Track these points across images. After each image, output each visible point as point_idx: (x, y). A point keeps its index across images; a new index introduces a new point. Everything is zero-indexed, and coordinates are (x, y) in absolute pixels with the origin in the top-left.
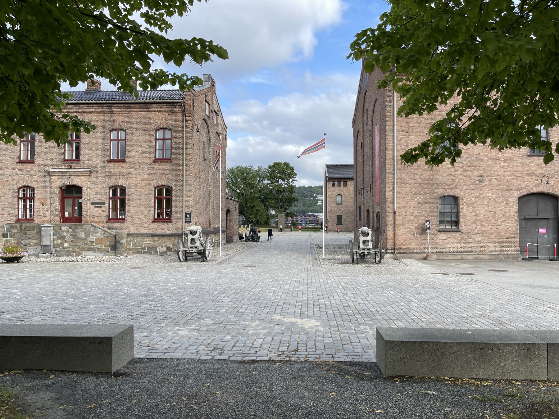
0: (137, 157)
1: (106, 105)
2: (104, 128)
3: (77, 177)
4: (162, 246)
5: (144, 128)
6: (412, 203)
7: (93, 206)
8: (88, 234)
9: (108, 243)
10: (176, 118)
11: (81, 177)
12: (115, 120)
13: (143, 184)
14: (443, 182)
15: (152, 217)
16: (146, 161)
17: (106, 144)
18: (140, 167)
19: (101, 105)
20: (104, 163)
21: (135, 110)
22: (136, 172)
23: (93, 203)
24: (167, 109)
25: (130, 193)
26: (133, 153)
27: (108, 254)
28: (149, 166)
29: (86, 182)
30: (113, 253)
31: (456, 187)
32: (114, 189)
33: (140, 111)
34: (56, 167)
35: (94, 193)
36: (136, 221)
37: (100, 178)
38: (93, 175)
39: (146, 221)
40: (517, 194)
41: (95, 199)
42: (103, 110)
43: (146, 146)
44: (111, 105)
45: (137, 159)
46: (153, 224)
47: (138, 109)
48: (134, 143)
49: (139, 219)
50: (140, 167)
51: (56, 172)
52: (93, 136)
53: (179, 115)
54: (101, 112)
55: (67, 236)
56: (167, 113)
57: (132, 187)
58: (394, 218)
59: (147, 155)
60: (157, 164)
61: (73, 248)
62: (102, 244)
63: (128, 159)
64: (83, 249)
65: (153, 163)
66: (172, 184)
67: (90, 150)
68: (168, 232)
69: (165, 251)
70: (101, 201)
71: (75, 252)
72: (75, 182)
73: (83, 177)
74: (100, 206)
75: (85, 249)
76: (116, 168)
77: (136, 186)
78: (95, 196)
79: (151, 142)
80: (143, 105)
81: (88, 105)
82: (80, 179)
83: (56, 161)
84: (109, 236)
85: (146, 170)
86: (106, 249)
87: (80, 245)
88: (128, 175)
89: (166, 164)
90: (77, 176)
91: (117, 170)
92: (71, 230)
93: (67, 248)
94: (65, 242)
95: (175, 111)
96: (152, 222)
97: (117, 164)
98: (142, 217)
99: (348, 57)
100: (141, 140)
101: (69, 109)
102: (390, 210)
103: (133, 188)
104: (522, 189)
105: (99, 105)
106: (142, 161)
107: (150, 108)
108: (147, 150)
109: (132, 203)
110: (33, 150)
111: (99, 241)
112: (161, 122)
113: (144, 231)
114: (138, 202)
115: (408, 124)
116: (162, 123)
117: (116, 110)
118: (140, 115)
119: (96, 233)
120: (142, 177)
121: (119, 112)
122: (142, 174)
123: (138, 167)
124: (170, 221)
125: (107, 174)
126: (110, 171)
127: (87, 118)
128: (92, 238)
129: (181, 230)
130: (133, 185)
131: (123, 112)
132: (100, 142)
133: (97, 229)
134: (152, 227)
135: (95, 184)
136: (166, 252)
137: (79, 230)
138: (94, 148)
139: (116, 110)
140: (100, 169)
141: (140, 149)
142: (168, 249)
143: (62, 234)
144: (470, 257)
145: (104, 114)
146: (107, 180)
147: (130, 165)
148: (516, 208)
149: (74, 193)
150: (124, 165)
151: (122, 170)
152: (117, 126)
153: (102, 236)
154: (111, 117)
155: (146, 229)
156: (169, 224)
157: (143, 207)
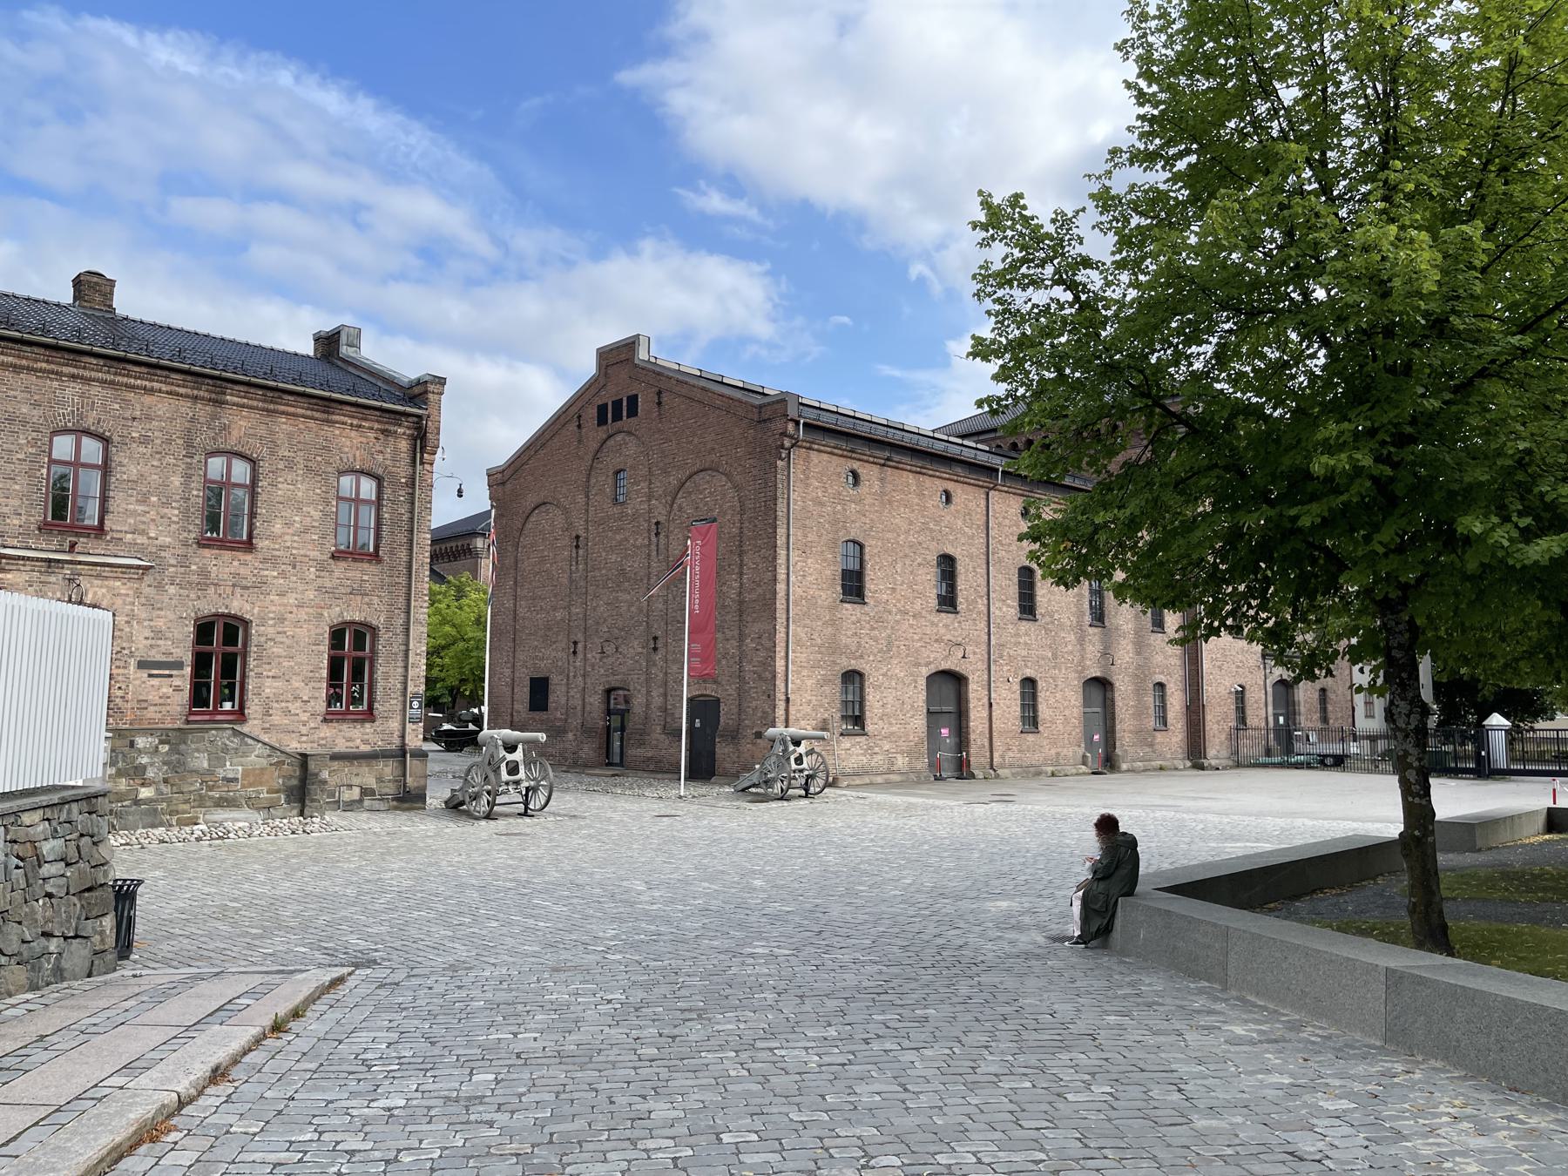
0: (287, 538)
1: (210, 382)
2: (189, 444)
3: (97, 582)
4: (350, 786)
5: (310, 464)
6: (809, 682)
7: (144, 674)
8: (218, 758)
9: (281, 781)
10: (396, 450)
11: (110, 583)
12: (224, 428)
13: (302, 614)
14: (846, 646)
15: (321, 706)
16: (312, 554)
17: (195, 493)
18: (294, 567)
19: (194, 379)
20: (185, 544)
21: (292, 410)
22: (281, 581)
23: (142, 665)
24: (376, 426)
25: (263, 639)
26: (278, 527)
27: (279, 812)
28: (322, 568)
29: (128, 599)
30: (293, 808)
31: (861, 657)
32: (204, 630)
33: (303, 416)
34: (15, 543)
35: (148, 633)
36: (276, 719)
37: (172, 590)
38: (148, 579)
39: (304, 717)
40: (925, 672)
41: (153, 653)
42: (195, 392)
43: (313, 513)
44: (224, 384)
45: (288, 544)
46: (324, 727)
47: (300, 411)
48: (281, 499)
49: (287, 712)
50: (294, 567)
51: (23, 558)
52: (155, 463)
53: (404, 445)
54: (187, 396)
55: (152, 764)
56: (372, 435)
57: (271, 622)
58: (787, 710)
59: (316, 537)
60: (343, 564)
61: (169, 801)
62: (261, 784)
63: (260, 543)
64: (201, 801)
65: (331, 561)
66: (378, 620)
67: (144, 500)
68: (365, 748)
69: (357, 797)
70: (170, 659)
71: (178, 812)
72: (90, 596)
73: (118, 584)
74: (167, 672)
75: (208, 804)
76: (223, 565)
77: (282, 620)
78: (149, 642)
79: (328, 504)
80: (320, 402)
81: (152, 371)
82: (107, 587)
83: (17, 522)
84: (283, 763)
85: (313, 577)
86: (272, 799)
87: (190, 792)
88: (260, 585)
89: (366, 565)
90: (98, 576)
91: (227, 570)
92: (166, 748)
93: (148, 801)
94: (143, 785)
95: (396, 432)
96: (325, 720)
97: (227, 555)
98: (295, 707)
99: (1028, 607)
100: (300, 494)
101: (84, 368)
102: (780, 696)
103: (274, 626)
104: (930, 663)
105: (189, 378)
106: (302, 552)
107: (333, 413)
108: (316, 524)
109: (267, 667)
110: (1329, 761)
111: (256, 777)
112: (358, 453)
113: (298, 746)
114: (285, 664)
115: (805, 536)
116: (358, 458)
117: (236, 399)
118: (301, 426)
119: (245, 755)
120: (299, 596)
121: (243, 406)
122: (301, 587)
123: (290, 568)
124: (370, 716)
125: (194, 578)
126: (204, 573)
127: (138, 407)
128: (232, 768)
129: (397, 741)
130: (271, 615)
131: (257, 408)
132: (177, 484)
133: (250, 741)
134: (322, 735)
135: (151, 605)
136: (361, 801)
137: (193, 746)
138: (154, 499)
139: (236, 399)
140: (173, 562)
141: (297, 519)
142: (366, 792)
143: (135, 759)
144: (879, 779)
145: (195, 403)
146: (193, 596)
147: (265, 560)
148: (923, 696)
149: (332, 652)
150: (249, 557)
151: (242, 571)
152: (232, 443)
153: (264, 762)
154: (214, 417)
155: (304, 738)
156: (368, 725)
157: (300, 678)
